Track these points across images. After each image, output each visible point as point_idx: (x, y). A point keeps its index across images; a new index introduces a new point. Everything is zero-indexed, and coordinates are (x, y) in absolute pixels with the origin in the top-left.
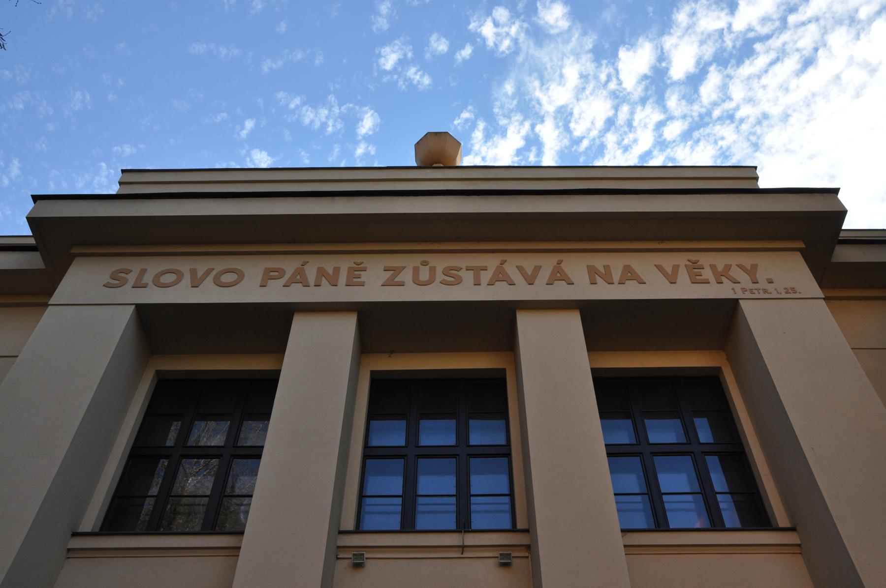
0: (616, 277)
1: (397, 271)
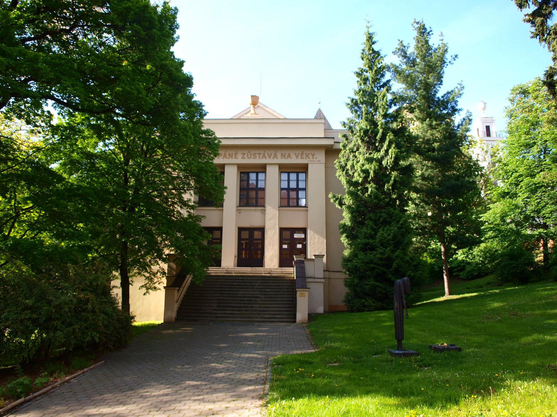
0: (286, 157)
1: (244, 154)
